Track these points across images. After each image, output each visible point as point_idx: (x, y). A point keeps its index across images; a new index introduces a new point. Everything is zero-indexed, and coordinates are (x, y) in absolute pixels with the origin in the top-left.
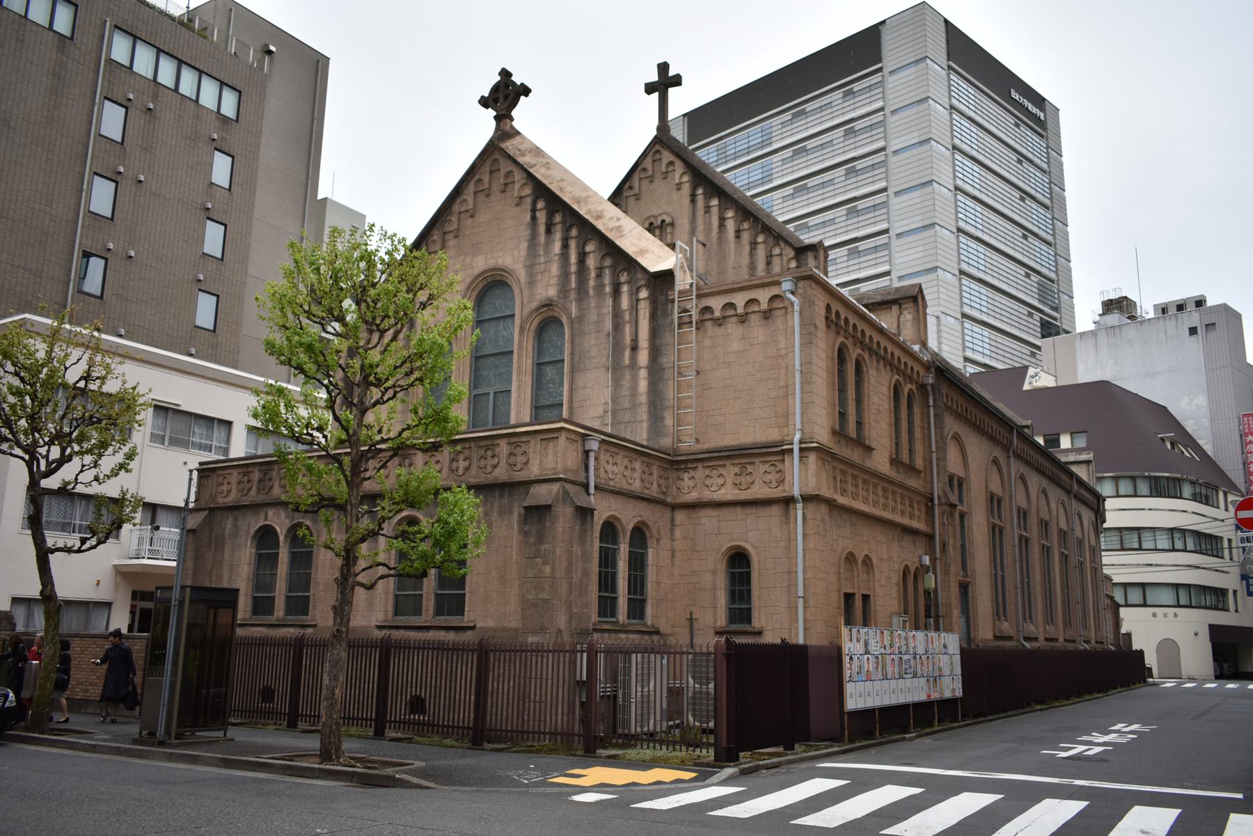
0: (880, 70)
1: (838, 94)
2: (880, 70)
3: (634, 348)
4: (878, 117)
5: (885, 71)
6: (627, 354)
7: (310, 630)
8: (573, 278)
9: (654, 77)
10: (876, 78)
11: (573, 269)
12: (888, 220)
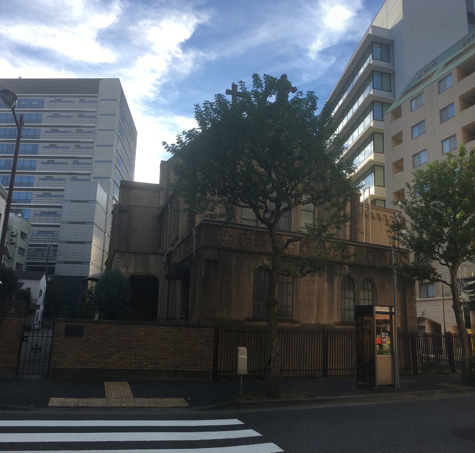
0: (97, 97)
1: (78, 99)
2: (97, 97)
7: (298, 325)
10: (95, 99)
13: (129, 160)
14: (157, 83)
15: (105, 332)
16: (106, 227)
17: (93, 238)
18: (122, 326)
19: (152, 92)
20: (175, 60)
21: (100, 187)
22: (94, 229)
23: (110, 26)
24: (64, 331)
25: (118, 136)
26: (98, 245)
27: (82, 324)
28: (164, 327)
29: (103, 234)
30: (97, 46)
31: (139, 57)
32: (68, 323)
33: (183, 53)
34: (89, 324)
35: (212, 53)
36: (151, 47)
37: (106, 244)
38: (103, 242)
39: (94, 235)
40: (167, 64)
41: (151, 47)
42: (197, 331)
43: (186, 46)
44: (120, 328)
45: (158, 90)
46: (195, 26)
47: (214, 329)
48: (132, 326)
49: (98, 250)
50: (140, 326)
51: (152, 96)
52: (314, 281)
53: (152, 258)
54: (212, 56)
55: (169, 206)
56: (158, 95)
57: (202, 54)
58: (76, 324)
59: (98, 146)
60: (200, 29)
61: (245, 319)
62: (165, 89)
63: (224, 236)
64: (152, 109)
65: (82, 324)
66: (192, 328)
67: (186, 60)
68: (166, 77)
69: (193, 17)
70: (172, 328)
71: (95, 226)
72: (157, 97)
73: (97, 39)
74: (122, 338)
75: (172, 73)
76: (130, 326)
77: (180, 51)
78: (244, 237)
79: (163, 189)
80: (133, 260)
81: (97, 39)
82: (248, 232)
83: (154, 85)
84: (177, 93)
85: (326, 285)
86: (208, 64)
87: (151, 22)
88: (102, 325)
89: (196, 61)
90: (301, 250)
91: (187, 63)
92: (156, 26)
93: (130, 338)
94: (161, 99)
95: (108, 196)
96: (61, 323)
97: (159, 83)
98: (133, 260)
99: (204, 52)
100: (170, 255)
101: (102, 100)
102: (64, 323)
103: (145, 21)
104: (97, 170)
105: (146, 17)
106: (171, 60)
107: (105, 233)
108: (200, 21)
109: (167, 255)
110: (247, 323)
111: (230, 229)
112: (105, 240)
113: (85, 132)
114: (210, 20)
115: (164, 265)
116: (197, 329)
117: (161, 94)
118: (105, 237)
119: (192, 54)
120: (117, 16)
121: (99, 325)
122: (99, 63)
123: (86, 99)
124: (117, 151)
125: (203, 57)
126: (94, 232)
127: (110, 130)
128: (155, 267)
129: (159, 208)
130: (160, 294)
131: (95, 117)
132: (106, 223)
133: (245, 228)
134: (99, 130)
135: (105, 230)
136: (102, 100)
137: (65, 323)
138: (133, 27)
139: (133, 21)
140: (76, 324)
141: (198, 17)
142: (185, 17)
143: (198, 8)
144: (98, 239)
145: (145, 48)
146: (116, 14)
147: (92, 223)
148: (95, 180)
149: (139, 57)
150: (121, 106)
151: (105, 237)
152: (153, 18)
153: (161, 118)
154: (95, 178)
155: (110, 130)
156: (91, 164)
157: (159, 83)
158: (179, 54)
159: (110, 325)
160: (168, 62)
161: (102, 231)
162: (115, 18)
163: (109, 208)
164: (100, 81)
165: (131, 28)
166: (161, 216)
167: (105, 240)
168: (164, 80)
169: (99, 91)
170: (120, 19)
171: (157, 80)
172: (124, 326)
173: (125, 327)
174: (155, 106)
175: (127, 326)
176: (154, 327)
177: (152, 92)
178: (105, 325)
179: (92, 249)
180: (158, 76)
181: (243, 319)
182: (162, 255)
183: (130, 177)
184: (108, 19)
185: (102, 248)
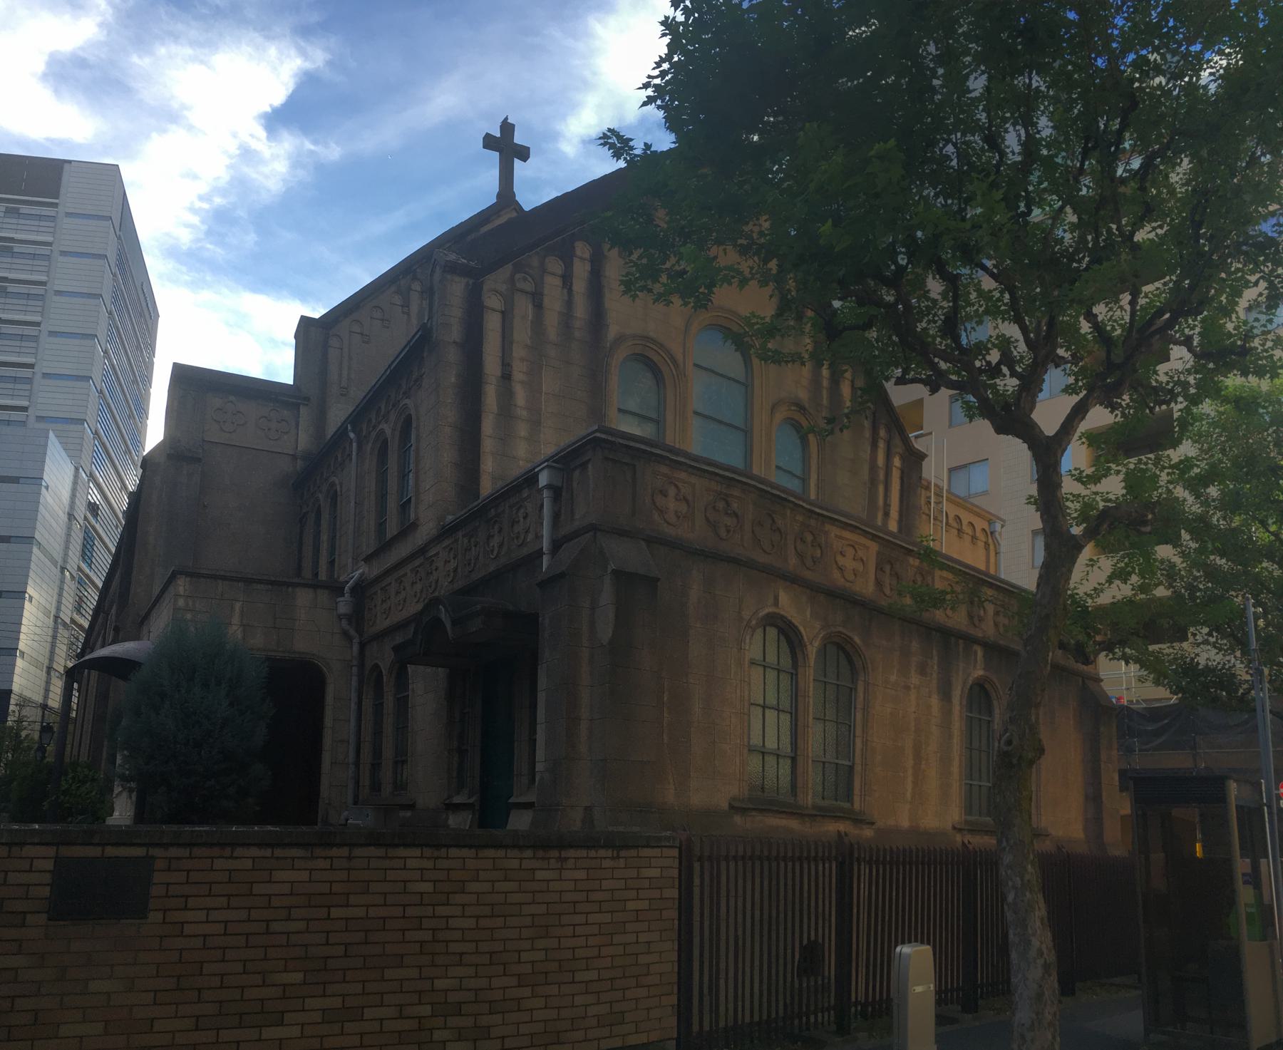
0: (56, 205)
2: (56, 205)
3: (887, 514)
4: (25, 373)
5: (60, 208)
6: (880, 515)
8: (825, 393)
9: (518, 139)
11: (825, 383)
12: (54, 233)
13: (135, 381)
14: (198, 204)
15: (257, 889)
16: (66, 555)
17: (30, 582)
18: (335, 852)
19: (187, 226)
20: (247, 154)
21: (57, 444)
22: (33, 558)
23: (82, 48)
24: (46, 891)
25: (110, 313)
26: (43, 601)
27: (139, 852)
28: (501, 853)
29: (57, 571)
30: (45, 93)
31: (154, 135)
32: (67, 851)
33: (268, 138)
34: (174, 852)
35: (333, 145)
36: (186, 113)
37: (64, 601)
38: (55, 597)
39: (31, 574)
40: (228, 162)
41: (186, 113)
42: (622, 863)
43: (277, 120)
44: (327, 864)
45: (203, 222)
46: (296, 75)
47: (675, 852)
48: (381, 852)
49: (41, 615)
50: (417, 852)
51: (185, 238)
52: (908, 688)
53: (303, 597)
54: (333, 152)
55: (352, 435)
56: (202, 236)
57: (309, 146)
58: (111, 851)
59: (52, 334)
60: (308, 83)
61: (731, 807)
62: (220, 221)
63: (664, 494)
64: (184, 269)
65: (139, 852)
66: (602, 853)
67: (275, 157)
68: (223, 192)
69: (293, 52)
70: (529, 853)
71: (35, 550)
72: (198, 240)
73: (45, 77)
74: (335, 912)
75: (240, 185)
76: (372, 851)
77: (262, 134)
78: (721, 505)
79: (307, 399)
80: (238, 606)
81: (45, 77)
82: (736, 493)
83: (193, 210)
84: (251, 238)
85: (935, 701)
86: (321, 169)
87: (189, 51)
88: (239, 851)
89: (297, 161)
90: (879, 583)
91: (277, 163)
92: (202, 62)
93: (373, 912)
94: (209, 246)
95: (77, 469)
96: (29, 851)
97: (206, 206)
98: (238, 606)
99: (315, 142)
100: (361, 590)
101: (68, 215)
102: (42, 851)
103: (174, 49)
104: (49, 398)
105: (176, 37)
106: (238, 152)
107: (63, 569)
108: (308, 65)
109: (353, 590)
110: (738, 819)
111: (683, 475)
112: (61, 589)
113: (18, 295)
114: (330, 63)
115: (344, 623)
116: (623, 853)
117: (209, 233)
118: (62, 581)
119: (288, 143)
120: (101, 25)
121: (228, 851)
122: (47, 139)
123: (25, 209)
124: (106, 352)
125: (312, 152)
126: (33, 566)
127: (90, 295)
128: (313, 628)
129: (294, 457)
130: (328, 721)
131: (48, 257)
132: (68, 535)
133: (727, 474)
134: (58, 293)
135: (65, 561)
136: (68, 215)
137: (51, 851)
138: (140, 57)
139: (142, 42)
140: (111, 851)
141: (303, 53)
142: (273, 51)
143: (305, 32)
144: (44, 586)
145: (169, 116)
146: (99, 19)
147: (30, 539)
148: (41, 425)
149: (154, 135)
150: (119, 238)
151: (62, 581)
152: (194, 43)
153: (206, 295)
154: (40, 419)
155: (90, 295)
156: (29, 381)
157: (206, 206)
158: (259, 139)
159: (279, 852)
160: (231, 157)
161: (55, 563)
162: (96, 30)
163: (77, 502)
164: (66, 166)
165: (135, 59)
166: (310, 480)
167: (61, 589)
168: (218, 200)
169: (63, 191)
170: (109, 34)
171: (201, 198)
172: (345, 851)
173: (350, 858)
174: (192, 260)
175: (358, 852)
176: (465, 852)
177: (187, 226)
178: (254, 852)
179: (26, 613)
180: (204, 188)
181: (725, 805)
182: (337, 590)
183: (135, 423)
184: (79, 32)
185: (53, 612)
